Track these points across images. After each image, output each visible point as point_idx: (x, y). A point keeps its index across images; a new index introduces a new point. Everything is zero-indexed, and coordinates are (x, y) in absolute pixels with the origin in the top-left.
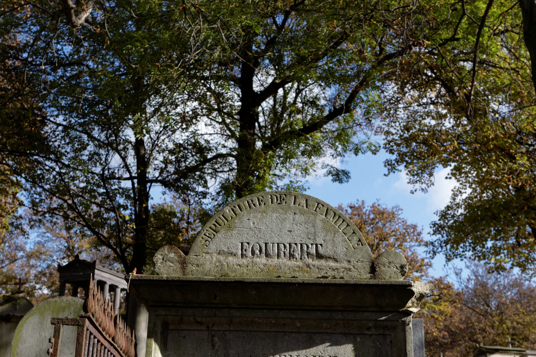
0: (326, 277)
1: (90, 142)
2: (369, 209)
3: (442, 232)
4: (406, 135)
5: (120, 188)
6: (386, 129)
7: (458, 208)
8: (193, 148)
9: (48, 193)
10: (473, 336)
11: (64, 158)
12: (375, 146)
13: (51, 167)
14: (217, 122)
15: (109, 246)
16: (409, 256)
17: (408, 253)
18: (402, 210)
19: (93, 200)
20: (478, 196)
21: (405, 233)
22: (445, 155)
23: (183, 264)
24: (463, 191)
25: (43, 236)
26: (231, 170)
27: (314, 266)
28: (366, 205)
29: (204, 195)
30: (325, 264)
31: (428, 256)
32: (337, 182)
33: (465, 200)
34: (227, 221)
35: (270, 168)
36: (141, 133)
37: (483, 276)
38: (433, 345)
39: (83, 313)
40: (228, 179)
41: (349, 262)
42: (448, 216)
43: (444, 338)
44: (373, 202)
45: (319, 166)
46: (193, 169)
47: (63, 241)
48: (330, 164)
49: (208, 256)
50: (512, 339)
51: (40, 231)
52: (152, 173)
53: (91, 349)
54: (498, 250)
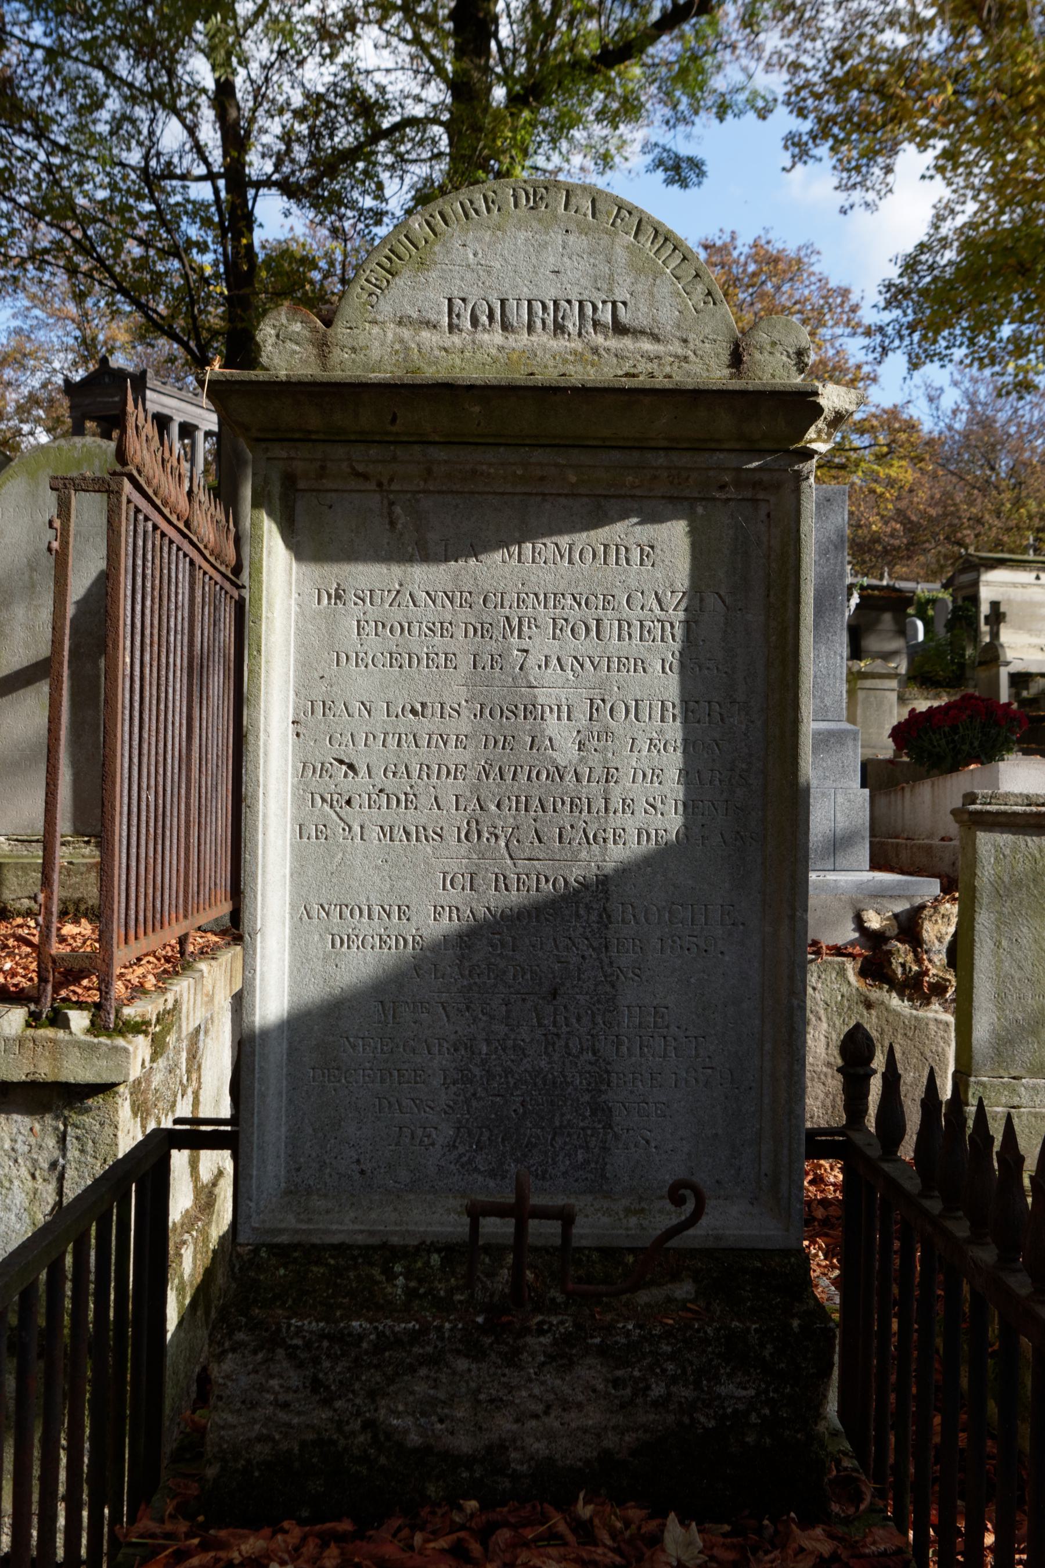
0: (634, 376)
1: (112, 90)
2: (746, 250)
3: (905, 304)
4: (838, 72)
5: (188, 201)
6: (792, 57)
7: (944, 247)
8: (349, 103)
9: (26, 215)
10: (955, 532)
11: (55, 128)
12: (764, 98)
13: (28, 152)
14: (404, 40)
15: (174, 337)
16: (829, 359)
17: (826, 351)
18: (818, 253)
19: (129, 231)
20: (991, 221)
21: (822, 307)
22: (923, 122)
23: (323, 346)
24: (958, 208)
25: (26, 317)
26: (438, 156)
27: (608, 350)
28: (739, 243)
29: (378, 217)
30: (631, 347)
31: (871, 357)
32: (676, 186)
33: (960, 231)
34: (417, 248)
35: (525, 153)
36: (228, 63)
37: (986, 404)
38: (870, 551)
39: (118, 468)
40: (429, 179)
41: (685, 341)
42: (919, 268)
43: (892, 535)
44: (756, 235)
45: (637, 147)
46: (351, 155)
47: (71, 327)
48: (661, 142)
49: (376, 330)
50: (1036, 539)
51: (18, 304)
52: (258, 165)
53: (140, 543)
54: (1023, 344)
